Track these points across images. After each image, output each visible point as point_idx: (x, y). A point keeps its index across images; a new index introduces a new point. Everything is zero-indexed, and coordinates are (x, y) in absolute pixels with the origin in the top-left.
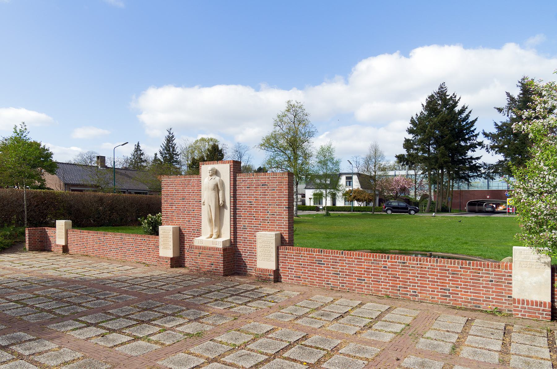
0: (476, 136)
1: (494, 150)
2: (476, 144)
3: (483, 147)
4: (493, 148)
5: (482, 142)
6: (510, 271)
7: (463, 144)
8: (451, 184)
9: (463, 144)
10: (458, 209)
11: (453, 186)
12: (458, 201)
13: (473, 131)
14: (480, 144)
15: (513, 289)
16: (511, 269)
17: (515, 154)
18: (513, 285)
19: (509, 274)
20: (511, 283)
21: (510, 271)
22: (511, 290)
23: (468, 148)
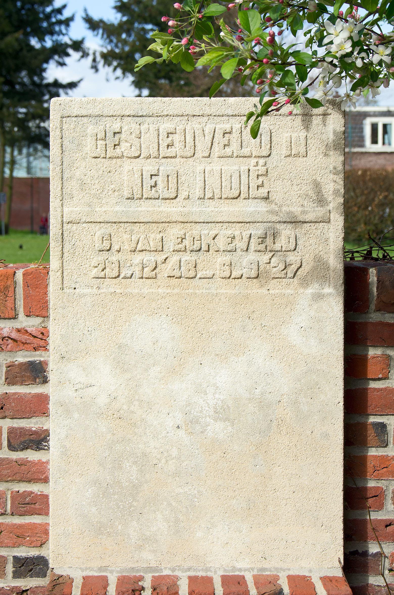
0: (67, 22)
1: (109, 65)
2: (67, 45)
3: (85, 55)
4: (108, 57)
5: (82, 42)
6: (31, 324)
7: (34, 42)
8: (8, 158)
9: (34, 42)
10: (27, 228)
11: (13, 162)
12: (27, 206)
13: (59, 11)
14: (77, 45)
15: (52, 490)
16: (39, 306)
17: (158, 78)
18: (53, 456)
19: (22, 357)
20: (39, 441)
21: (31, 324)
22: (39, 504)
23: (47, 55)
